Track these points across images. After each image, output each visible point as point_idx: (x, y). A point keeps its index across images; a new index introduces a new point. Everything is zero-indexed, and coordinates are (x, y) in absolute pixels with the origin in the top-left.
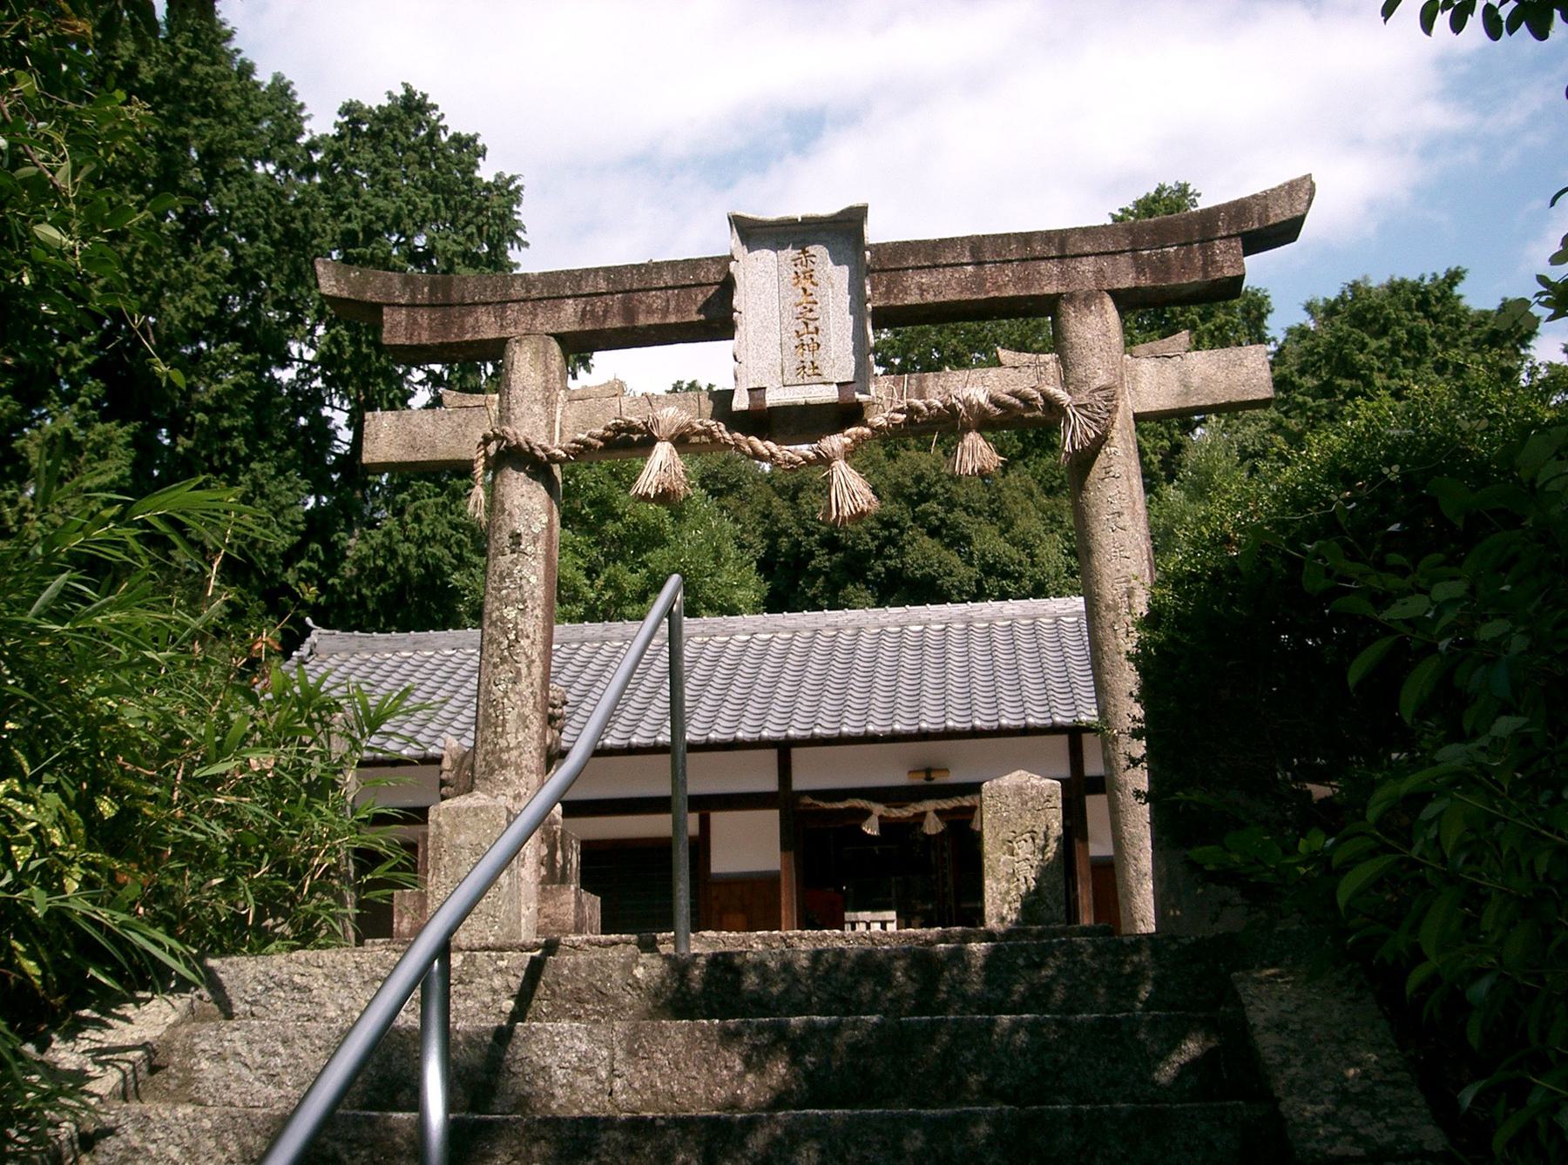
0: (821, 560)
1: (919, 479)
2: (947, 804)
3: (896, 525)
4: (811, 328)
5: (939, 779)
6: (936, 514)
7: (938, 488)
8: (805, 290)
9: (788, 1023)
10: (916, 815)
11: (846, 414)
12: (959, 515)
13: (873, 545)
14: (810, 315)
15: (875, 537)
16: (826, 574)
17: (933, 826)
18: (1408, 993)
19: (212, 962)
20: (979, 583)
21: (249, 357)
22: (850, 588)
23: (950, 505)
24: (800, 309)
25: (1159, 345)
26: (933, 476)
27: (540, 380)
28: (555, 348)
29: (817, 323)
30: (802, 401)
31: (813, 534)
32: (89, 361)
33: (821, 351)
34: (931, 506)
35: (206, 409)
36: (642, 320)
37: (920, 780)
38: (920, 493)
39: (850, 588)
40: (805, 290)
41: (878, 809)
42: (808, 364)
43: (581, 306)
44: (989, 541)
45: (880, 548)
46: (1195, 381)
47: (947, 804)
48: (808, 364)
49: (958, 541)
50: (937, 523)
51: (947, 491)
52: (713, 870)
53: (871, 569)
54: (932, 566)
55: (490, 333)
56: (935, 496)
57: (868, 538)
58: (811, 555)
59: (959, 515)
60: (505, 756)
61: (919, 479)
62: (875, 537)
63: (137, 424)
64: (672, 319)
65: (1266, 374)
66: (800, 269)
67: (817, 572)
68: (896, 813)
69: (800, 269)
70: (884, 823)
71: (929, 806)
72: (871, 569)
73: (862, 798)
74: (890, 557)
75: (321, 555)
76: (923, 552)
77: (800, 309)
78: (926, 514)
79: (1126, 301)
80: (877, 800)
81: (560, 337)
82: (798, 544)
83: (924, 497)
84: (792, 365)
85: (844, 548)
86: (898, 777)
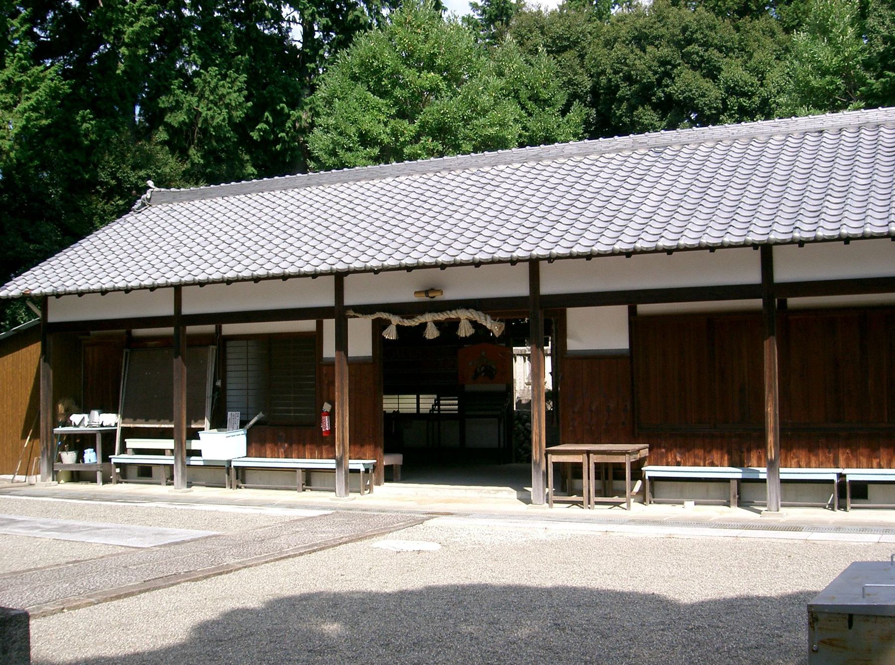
0: (625, 90)
1: (684, 29)
2: (441, 317)
3: (669, 63)
5: (439, 297)
6: (697, 53)
7: (698, 35)
10: (421, 324)
12: (714, 54)
13: (653, 79)
15: (655, 73)
16: (628, 100)
17: (432, 333)
20: (724, 101)
21: (149, 8)
22: (640, 109)
23: (706, 45)
26: (694, 26)
31: (618, 73)
32: (23, 29)
34: (693, 48)
35: (127, 46)
37: (423, 298)
38: (685, 39)
39: (640, 109)
41: (395, 320)
44: (734, 70)
45: (659, 81)
47: (441, 317)
49: (712, 73)
50: (698, 59)
51: (705, 36)
52: (324, 356)
53: (654, 95)
54: (691, 91)
56: (696, 41)
57: (650, 73)
58: (617, 87)
59: (714, 54)
61: (684, 29)
62: (655, 73)
67: (621, 100)
68: (407, 323)
70: (399, 328)
71: (428, 318)
72: (654, 95)
73: (384, 311)
74: (667, 86)
75: (270, 119)
76: (686, 81)
78: (690, 54)
80: (395, 313)
82: (610, 80)
83: (689, 42)
85: (636, 82)
86: (407, 296)
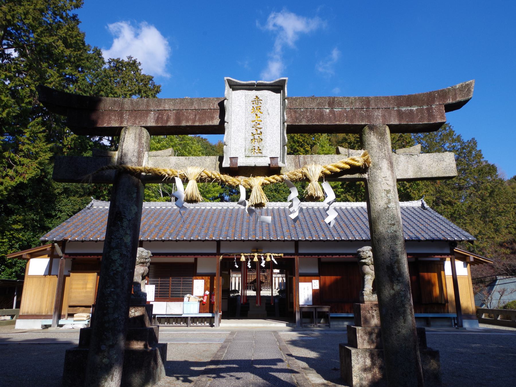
4: (259, 132)
8: (257, 115)
9: (199, 123)
11: (272, 170)
14: (258, 126)
18: (302, 301)
19: (339, 147)
24: (254, 123)
25: (407, 150)
27: (136, 146)
28: (145, 132)
29: (261, 130)
30: (253, 165)
33: (263, 142)
36: (184, 124)
40: (257, 115)
42: (256, 148)
43: (157, 115)
46: (424, 167)
48: (256, 148)
55: (115, 124)
60: (107, 325)
63: (333, 278)
64: (197, 124)
65: (454, 164)
66: (255, 106)
69: (255, 106)
77: (254, 123)
79: (394, 129)
81: (147, 128)
84: (249, 146)
